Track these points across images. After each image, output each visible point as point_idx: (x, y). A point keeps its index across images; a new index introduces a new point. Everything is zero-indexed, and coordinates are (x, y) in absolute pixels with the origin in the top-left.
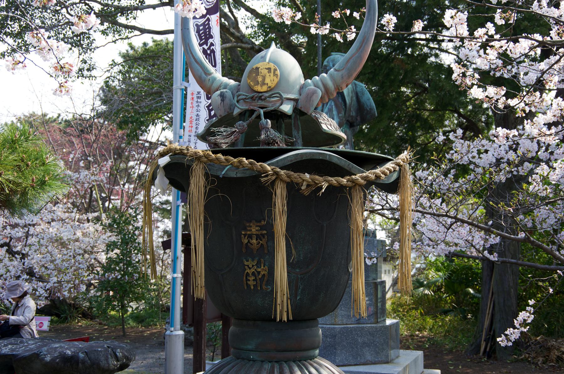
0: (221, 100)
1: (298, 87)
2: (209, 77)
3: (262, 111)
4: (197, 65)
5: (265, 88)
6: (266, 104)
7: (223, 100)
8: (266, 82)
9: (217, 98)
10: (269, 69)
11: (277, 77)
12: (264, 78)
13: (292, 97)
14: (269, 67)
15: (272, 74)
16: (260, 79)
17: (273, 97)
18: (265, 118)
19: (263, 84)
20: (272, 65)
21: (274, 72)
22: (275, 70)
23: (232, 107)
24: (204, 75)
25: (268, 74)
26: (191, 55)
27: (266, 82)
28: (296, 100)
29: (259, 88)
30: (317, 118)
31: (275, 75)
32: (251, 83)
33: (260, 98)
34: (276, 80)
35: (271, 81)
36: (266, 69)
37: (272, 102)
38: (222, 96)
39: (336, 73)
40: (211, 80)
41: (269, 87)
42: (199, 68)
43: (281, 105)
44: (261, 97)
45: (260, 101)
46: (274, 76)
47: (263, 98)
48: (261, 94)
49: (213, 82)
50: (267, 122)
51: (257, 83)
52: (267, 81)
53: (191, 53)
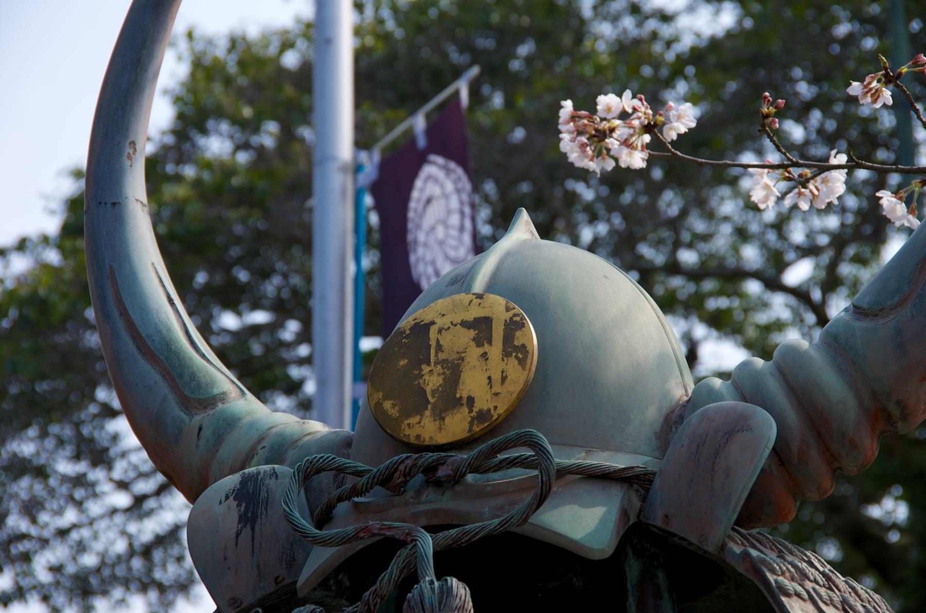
0: (243, 519)
1: (652, 414)
2: (198, 418)
3: (427, 543)
4: (144, 366)
5: (457, 426)
6: (463, 506)
7: (248, 519)
8: (464, 391)
9: (219, 510)
10: (481, 327)
11: (522, 362)
12: (454, 371)
13: (618, 461)
14: (481, 313)
15: (495, 349)
16: (432, 380)
17: (500, 466)
18: (441, 574)
19: (450, 399)
20: (497, 307)
21: (508, 338)
22: (514, 326)
23: (297, 545)
24: (176, 411)
25: (474, 352)
26: (120, 325)
27: (464, 391)
28: (634, 481)
29: (425, 428)
30: (756, 568)
31: (514, 349)
32: (387, 405)
33: (433, 479)
34: (518, 377)
35: (488, 382)
36: (465, 324)
37: (498, 491)
38: (250, 497)
39: (861, 325)
40: (207, 433)
41: (483, 416)
42: (154, 377)
43: (541, 500)
44: (431, 469)
45: (430, 494)
46: (506, 354)
47: (442, 472)
48: (430, 456)
49: (219, 439)
50: (446, 592)
51: (416, 402)
52: (473, 383)
53: (124, 314)
